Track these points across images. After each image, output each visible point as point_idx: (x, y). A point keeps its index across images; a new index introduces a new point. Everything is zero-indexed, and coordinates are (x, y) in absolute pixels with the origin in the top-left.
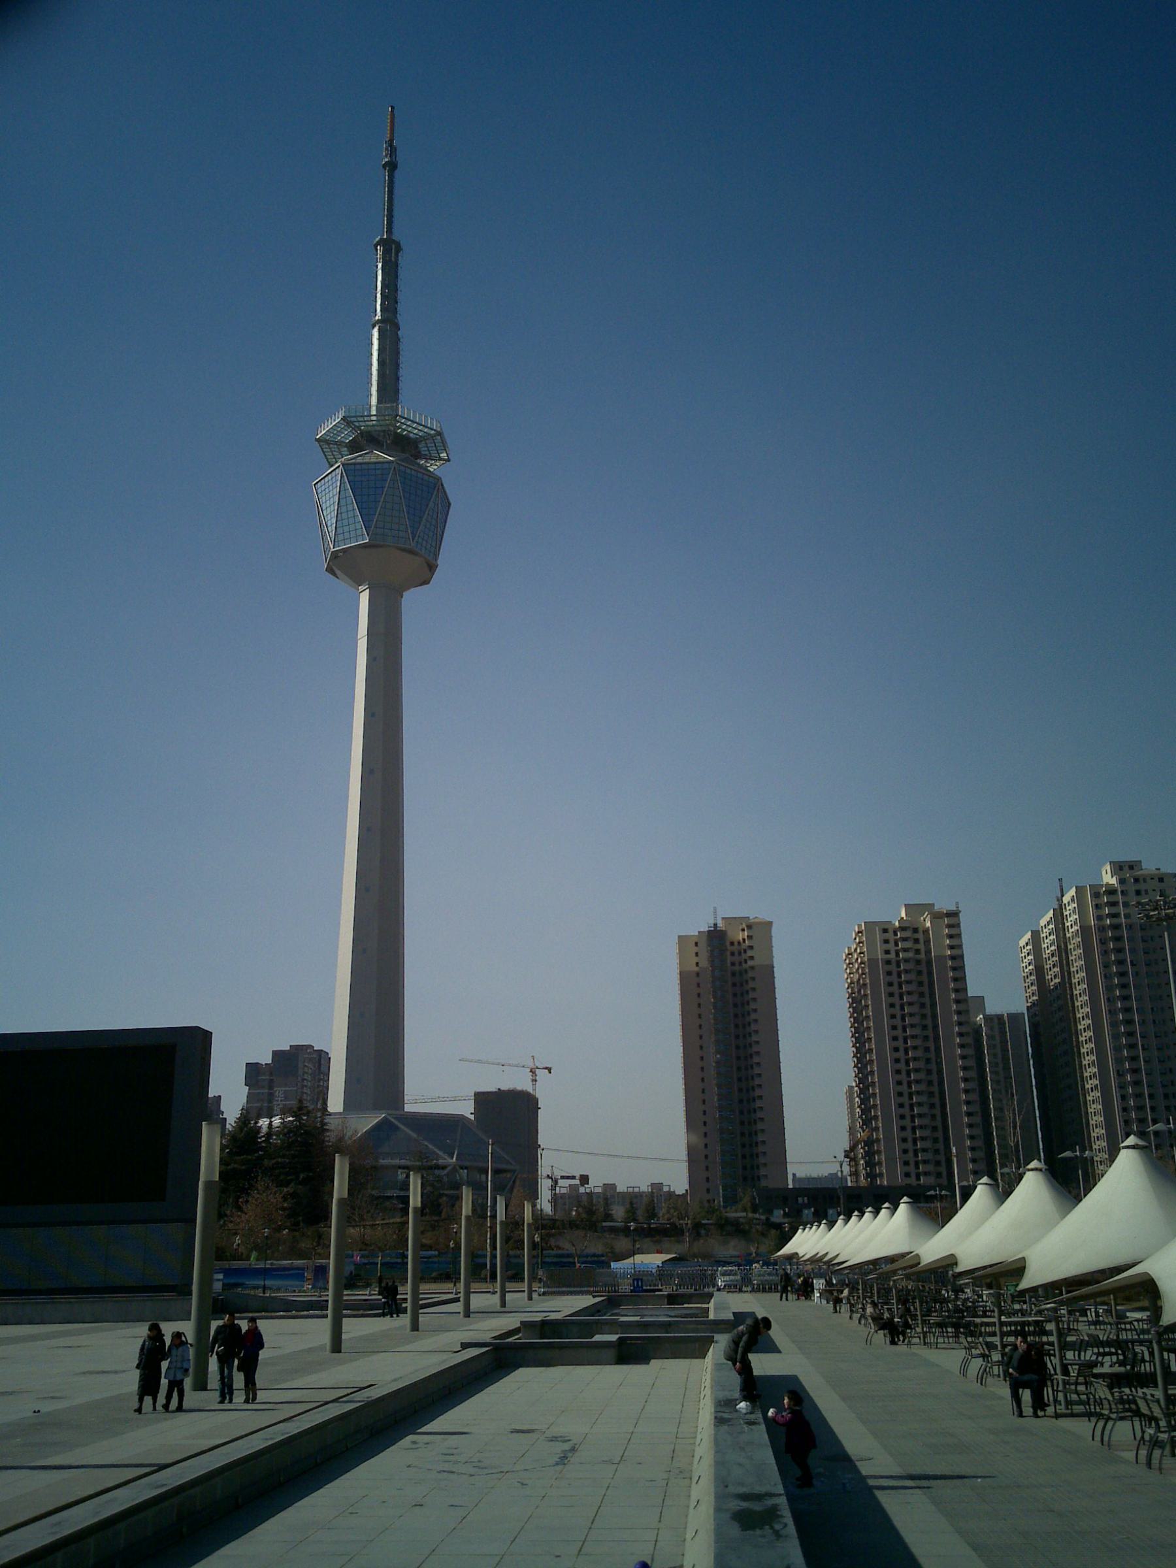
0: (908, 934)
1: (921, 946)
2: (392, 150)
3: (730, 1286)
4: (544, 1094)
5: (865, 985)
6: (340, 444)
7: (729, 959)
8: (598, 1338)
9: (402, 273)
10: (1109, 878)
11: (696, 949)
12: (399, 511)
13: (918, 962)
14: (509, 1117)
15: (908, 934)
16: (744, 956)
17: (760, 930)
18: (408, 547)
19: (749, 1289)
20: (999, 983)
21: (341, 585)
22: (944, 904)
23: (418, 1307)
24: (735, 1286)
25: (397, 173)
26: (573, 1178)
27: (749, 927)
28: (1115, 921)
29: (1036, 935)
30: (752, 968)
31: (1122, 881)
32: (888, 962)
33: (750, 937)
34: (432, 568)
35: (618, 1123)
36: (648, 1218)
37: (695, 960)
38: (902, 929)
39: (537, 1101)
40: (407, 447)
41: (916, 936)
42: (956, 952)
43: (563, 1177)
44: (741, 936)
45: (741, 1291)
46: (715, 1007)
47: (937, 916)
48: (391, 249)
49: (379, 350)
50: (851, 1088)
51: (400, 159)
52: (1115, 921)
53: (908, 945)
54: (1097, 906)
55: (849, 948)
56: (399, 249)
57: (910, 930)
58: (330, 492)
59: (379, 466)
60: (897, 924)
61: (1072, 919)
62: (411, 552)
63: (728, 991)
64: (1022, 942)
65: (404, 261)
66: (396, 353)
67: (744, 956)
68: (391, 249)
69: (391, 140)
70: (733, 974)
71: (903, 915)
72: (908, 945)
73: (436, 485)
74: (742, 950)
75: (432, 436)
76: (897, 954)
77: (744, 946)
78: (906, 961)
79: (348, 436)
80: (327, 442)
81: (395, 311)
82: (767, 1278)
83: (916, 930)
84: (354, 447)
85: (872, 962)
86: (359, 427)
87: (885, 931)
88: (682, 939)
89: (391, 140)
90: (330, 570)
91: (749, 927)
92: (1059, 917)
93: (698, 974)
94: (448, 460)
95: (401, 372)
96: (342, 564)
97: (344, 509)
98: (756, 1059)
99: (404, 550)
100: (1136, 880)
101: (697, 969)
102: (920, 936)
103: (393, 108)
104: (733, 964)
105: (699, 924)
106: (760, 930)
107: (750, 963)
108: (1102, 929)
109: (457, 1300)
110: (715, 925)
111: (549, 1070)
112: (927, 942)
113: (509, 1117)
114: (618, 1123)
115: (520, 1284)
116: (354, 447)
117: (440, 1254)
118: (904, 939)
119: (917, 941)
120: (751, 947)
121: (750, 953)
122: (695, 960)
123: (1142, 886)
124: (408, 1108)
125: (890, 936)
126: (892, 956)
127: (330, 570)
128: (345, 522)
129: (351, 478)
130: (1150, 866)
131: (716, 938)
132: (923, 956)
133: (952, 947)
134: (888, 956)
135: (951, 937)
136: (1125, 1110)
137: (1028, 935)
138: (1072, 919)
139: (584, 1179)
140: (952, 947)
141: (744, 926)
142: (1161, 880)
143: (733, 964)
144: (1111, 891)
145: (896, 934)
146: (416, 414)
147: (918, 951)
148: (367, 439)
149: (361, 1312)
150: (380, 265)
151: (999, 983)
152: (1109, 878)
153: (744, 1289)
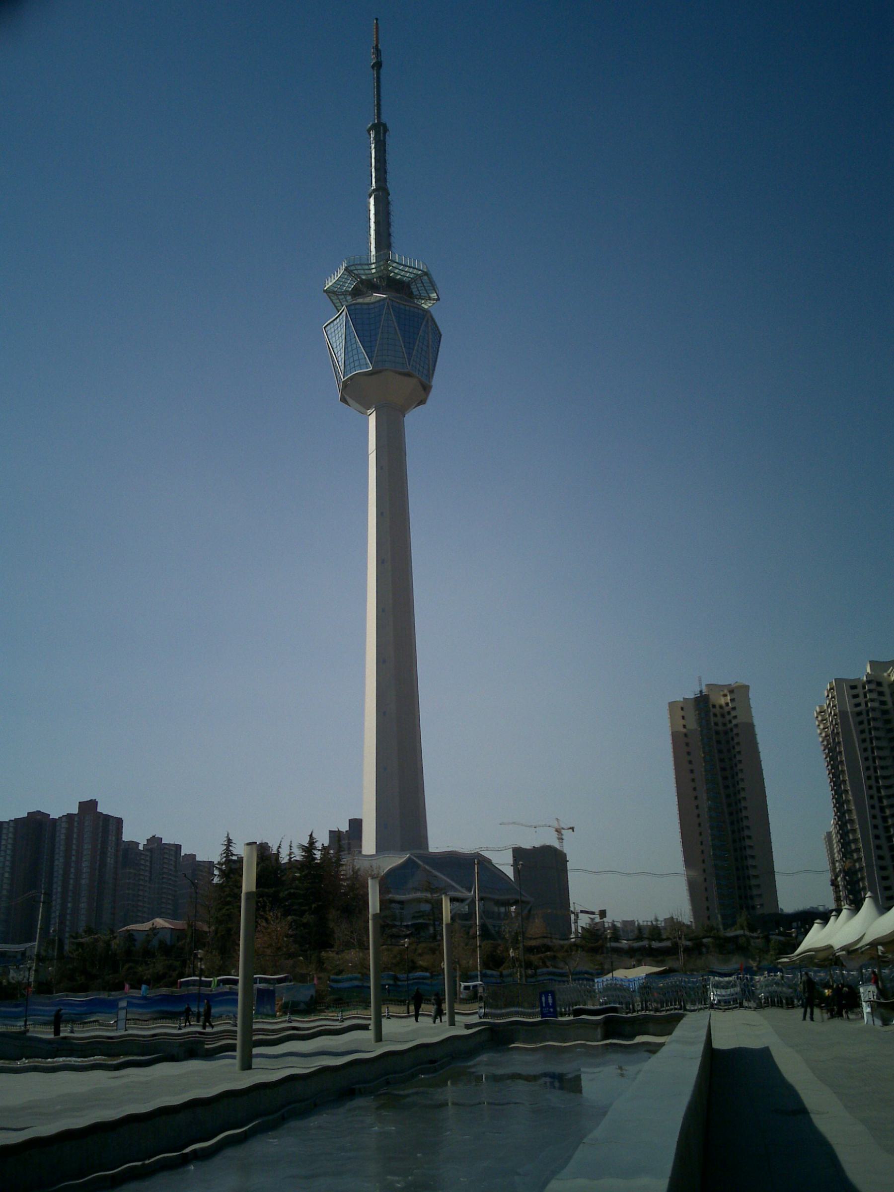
0: (873, 686)
2: (378, 52)
3: (727, 1002)
4: (568, 848)
5: (838, 733)
6: (345, 293)
7: (713, 719)
8: (639, 1039)
9: (389, 149)
11: (682, 713)
12: (397, 338)
14: (544, 868)
15: (873, 686)
16: (728, 718)
17: (739, 692)
18: (406, 370)
19: (752, 1004)
21: (351, 412)
23: (250, 1044)
24: (735, 1001)
25: (383, 71)
26: (593, 913)
27: (731, 692)
30: (736, 726)
33: (732, 700)
34: (426, 388)
35: (632, 869)
36: (648, 943)
37: (683, 722)
39: (565, 855)
41: (880, 689)
43: (582, 912)
44: (722, 701)
45: (741, 1006)
46: (705, 762)
48: (380, 129)
49: (375, 214)
50: (829, 834)
51: (384, 58)
55: (821, 707)
56: (386, 130)
57: (875, 682)
58: (337, 333)
59: (377, 305)
60: (865, 678)
62: (408, 375)
63: (715, 753)
65: (390, 141)
66: (388, 214)
67: (728, 718)
68: (380, 129)
69: (377, 45)
70: (717, 733)
71: (869, 670)
73: (426, 315)
74: (725, 713)
75: (420, 276)
76: (867, 705)
77: (727, 709)
79: (350, 285)
80: (334, 293)
81: (385, 181)
82: (775, 987)
83: (879, 684)
85: (843, 714)
86: (358, 276)
87: (853, 687)
88: (672, 705)
89: (377, 45)
90: (343, 400)
91: (731, 692)
93: (686, 735)
94: (438, 299)
95: (393, 229)
96: (354, 391)
97: (349, 344)
98: (744, 813)
99: (400, 373)
101: (684, 730)
103: (377, 19)
104: (716, 724)
106: (739, 692)
107: (734, 722)
109: (365, 1027)
110: (701, 692)
113: (544, 868)
114: (632, 869)
115: (365, 1012)
116: (356, 292)
117: (432, 976)
120: (734, 709)
121: (733, 713)
122: (683, 722)
124: (432, 849)
125: (860, 691)
127: (343, 400)
128: (350, 354)
129: (353, 317)
131: (702, 702)
134: (858, 709)
139: (603, 914)
141: (726, 692)
143: (716, 724)
145: (864, 687)
146: (406, 262)
148: (366, 286)
149: (122, 1059)
150: (373, 146)
153: (745, 1004)
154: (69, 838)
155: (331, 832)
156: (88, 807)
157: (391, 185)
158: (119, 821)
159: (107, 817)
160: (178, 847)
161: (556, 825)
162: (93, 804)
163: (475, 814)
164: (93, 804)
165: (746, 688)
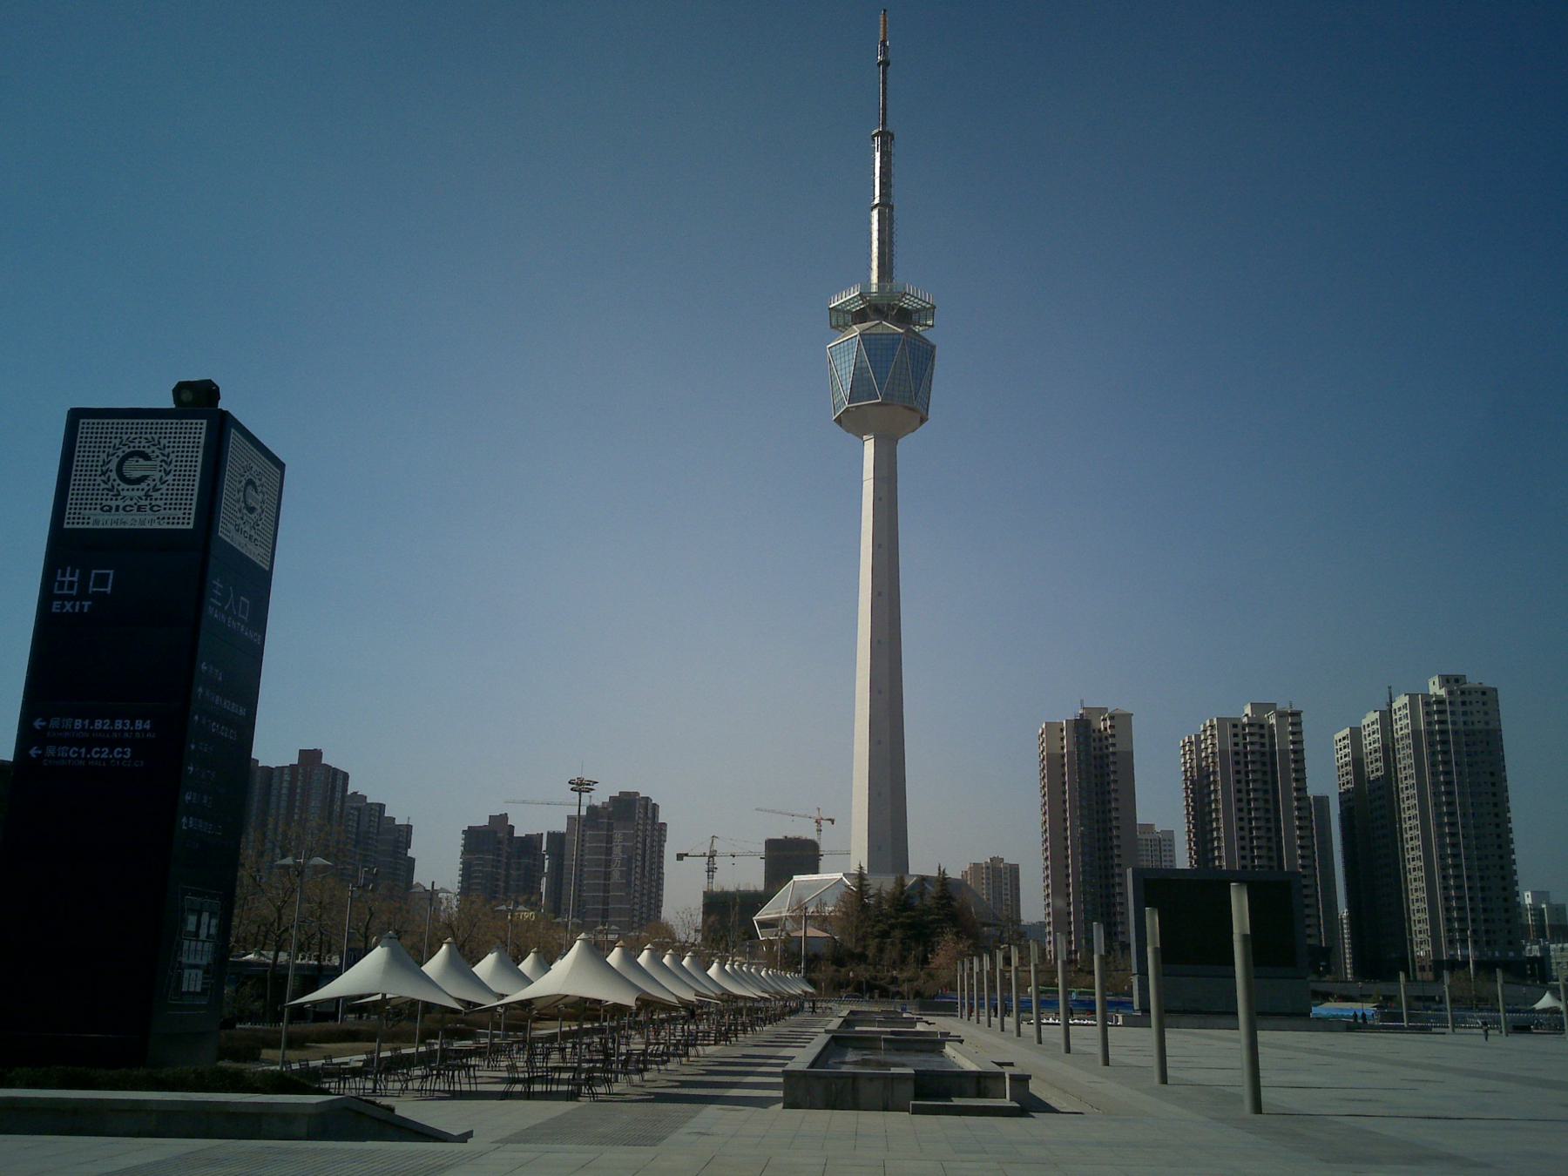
0: (1254, 730)
1: (1266, 741)
10: (1436, 689)
13: (1263, 754)
17: (1122, 721)
20: (1325, 778)
22: (1283, 706)
27: (1112, 718)
28: (1443, 727)
29: (1356, 734)
30: (1114, 753)
31: (1450, 693)
32: (1237, 753)
38: (1250, 725)
40: (904, 316)
42: (1298, 747)
47: (1281, 715)
52: (1443, 727)
53: (1256, 739)
54: (1428, 714)
57: (1258, 726)
61: (1402, 726)
64: (1338, 736)
65: (897, 149)
68: (887, 138)
71: (1248, 710)
72: (1256, 739)
74: (1102, 737)
78: (1253, 753)
83: (1262, 727)
84: (860, 317)
87: (1235, 726)
91: (1112, 718)
92: (1387, 719)
96: (853, 422)
100: (1463, 693)
102: (1266, 731)
105: (1066, 714)
106: (1122, 721)
108: (1431, 733)
111: (833, 821)
112: (1272, 736)
118: (1251, 734)
119: (1262, 736)
120: (1113, 736)
123: (1467, 698)
126: (1241, 747)
130: (1473, 680)
131: (1082, 726)
132: (1267, 749)
133: (1293, 743)
135: (1293, 733)
136: (1445, 888)
137: (1347, 731)
138: (1402, 726)
140: (1293, 743)
142: (1484, 693)
144: (1440, 701)
146: (915, 294)
147: (1263, 745)
151: (1325, 778)
152: (1436, 689)
154: (292, 790)
155: (301, 751)
156: (310, 757)
157: (896, 201)
158: (346, 776)
159: (336, 771)
160: (382, 807)
161: (816, 815)
162: (317, 754)
163: (939, 849)
164: (317, 754)
165: (1128, 717)
